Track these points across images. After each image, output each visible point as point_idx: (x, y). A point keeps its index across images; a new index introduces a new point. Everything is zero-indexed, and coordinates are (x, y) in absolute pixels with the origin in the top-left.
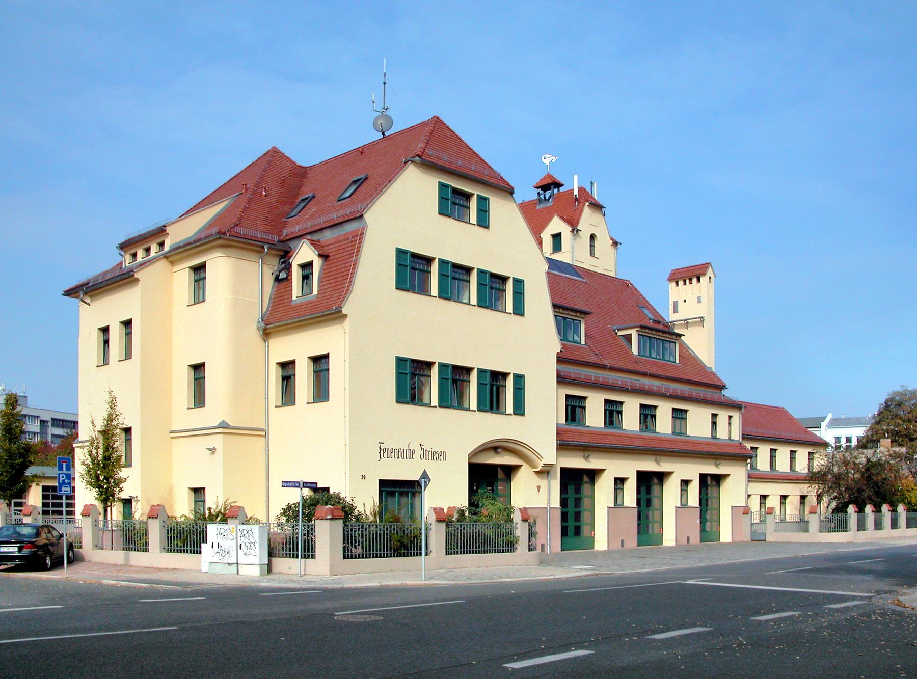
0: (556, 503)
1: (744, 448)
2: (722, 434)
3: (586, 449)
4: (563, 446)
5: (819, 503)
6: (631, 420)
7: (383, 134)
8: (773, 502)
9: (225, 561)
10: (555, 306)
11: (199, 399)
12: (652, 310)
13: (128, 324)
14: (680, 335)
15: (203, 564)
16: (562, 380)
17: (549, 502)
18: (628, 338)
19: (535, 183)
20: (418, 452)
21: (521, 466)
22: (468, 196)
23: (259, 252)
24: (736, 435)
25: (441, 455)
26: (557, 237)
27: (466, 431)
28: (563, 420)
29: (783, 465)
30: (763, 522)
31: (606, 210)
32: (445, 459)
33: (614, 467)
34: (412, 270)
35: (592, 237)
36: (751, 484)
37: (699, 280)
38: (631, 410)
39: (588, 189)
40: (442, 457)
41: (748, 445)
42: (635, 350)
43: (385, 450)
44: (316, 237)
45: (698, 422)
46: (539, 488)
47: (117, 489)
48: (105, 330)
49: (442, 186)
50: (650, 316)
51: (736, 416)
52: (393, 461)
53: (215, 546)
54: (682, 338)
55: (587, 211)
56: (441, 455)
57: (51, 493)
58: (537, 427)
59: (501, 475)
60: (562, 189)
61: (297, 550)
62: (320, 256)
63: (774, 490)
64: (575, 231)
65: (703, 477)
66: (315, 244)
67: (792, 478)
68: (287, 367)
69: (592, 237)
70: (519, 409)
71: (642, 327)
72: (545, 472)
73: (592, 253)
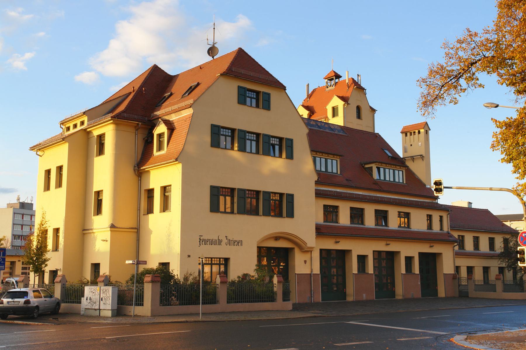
0: (317, 270)
1: (452, 236)
2: (436, 228)
6: (370, 221)
7: (213, 57)
9: (93, 308)
16: (319, 194)
20: (225, 241)
24: (446, 228)
25: (239, 243)
27: (261, 228)
29: (484, 247)
32: (241, 245)
33: (358, 248)
38: (393, 212)
39: (356, 79)
40: (240, 244)
41: (456, 234)
46: (305, 262)
47: (43, 266)
50: (390, 155)
52: (208, 246)
56: (239, 243)
60: (341, 79)
65: (421, 255)
70: (290, 214)
73: (359, 117)
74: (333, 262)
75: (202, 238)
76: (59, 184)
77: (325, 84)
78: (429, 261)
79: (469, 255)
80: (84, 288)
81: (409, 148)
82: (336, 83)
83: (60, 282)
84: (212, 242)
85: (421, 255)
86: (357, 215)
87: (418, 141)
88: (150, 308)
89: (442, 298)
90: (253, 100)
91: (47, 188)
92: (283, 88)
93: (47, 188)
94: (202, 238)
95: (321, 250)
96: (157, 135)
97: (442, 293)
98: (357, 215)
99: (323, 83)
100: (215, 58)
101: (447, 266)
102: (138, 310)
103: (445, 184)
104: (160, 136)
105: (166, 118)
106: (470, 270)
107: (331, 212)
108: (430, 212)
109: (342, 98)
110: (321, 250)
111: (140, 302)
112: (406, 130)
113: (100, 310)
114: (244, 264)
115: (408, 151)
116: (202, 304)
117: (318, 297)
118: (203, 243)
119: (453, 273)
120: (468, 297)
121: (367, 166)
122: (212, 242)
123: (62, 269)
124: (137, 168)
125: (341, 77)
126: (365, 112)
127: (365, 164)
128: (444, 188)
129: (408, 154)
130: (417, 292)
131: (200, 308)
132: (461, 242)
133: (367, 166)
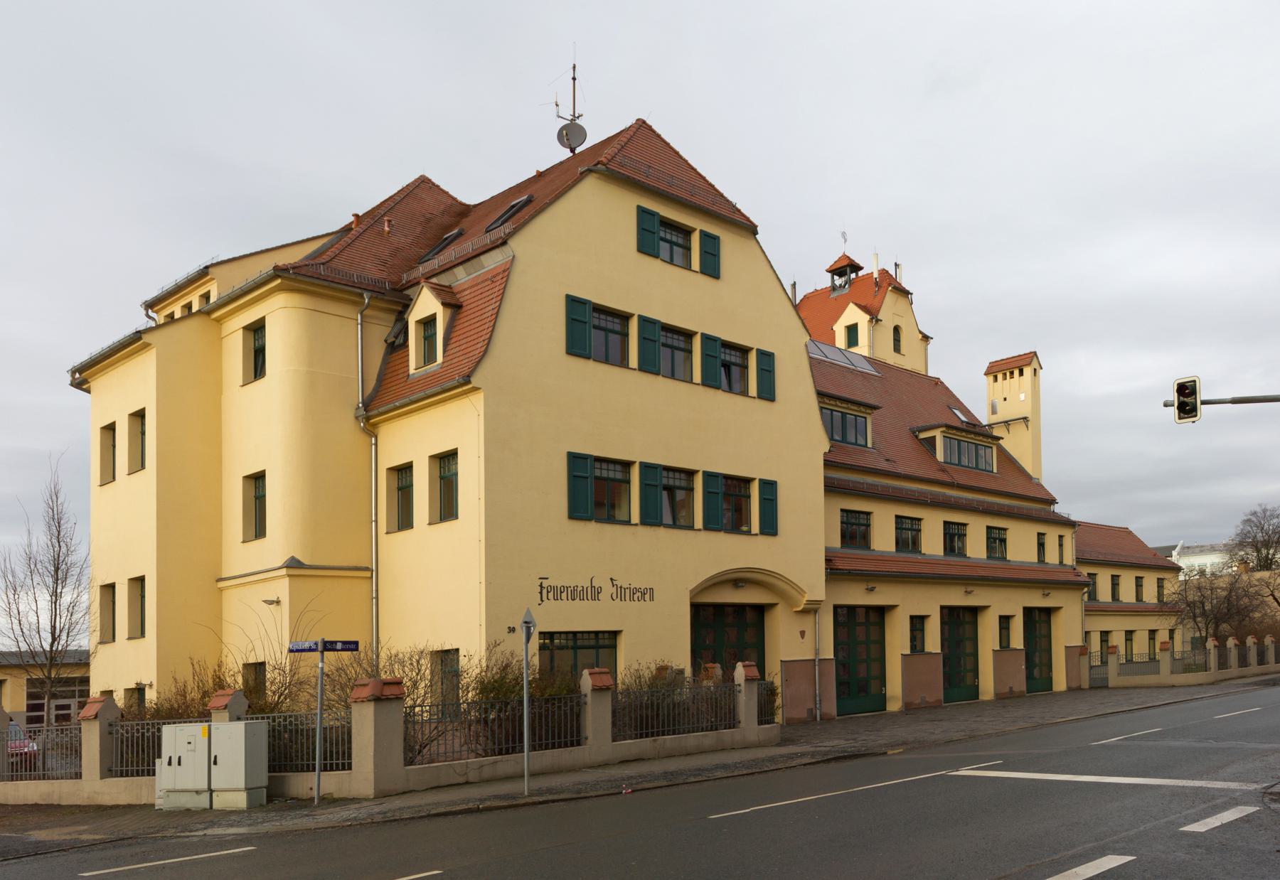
2: (1052, 557)
3: (871, 577)
4: (835, 572)
5: (1171, 638)
7: (572, 151)
8: (1118, 640)
10: (820, 394)
11: (257, 526)
12: (966, 411)
13: (140, 415)
14: (999, 438)
15: (158, 793)
16: (832, 488)
17: (817, 652)
18: (932, 441)
19: (828, 267)
20: (608, 590)
21: (776, 604)
22: (687, 232)
23: (354, 303)
24: (1069, 559)
25: (645, 594)
26: (852, 331)
27: (692, 558)
28: (836, 543)
29: (1127, 594)
30: (1104, 662)
31: (914, 298)
32: (652, 599)
33: (907, 602)
34: (593, 329)
35: (897, 330)
36: (1088, 618)
37: (1021, 373)
39: (892, 272)
40: (647, 597)
41: (1085, 571)
42: (940, 456)
43: (551, 589)
44: (443, 280)
45: (1021, 544)
46: (803, 634)
48: (110, 429)
49: (642, 211)
50: (963, 418)
51: (1068, 535)
52: (565, 605)
53: (175, 761)
54: (1001, 442)
55: (890, 298)
57: (77, 688)
58: (798, 549)
59: (750, 616)
60: (861, 273)
61: (314, 759)
62: (445, 304)
63: (1117, 626)
64: (874, 319)
65: (1028, 612)
66: (440, 291)
67: (1139, 609)
68: (403, 472)
69: (897, 330)
70: (770, 526)
71: (948, 427)
72: (811, 609)
73: (897, 348)
74: (859, 629)
75: (545, 584)
76: (138, 463)
77: (829, 284)
78: (1038, 620)
79: (1104, 611)
80: (159, 730)
81: (1001, 406)
82: (849, 282)
83: (96, 717)
84: (575, 594)
85: (1028, 612)
86: (908, 534)
87: (1016, 392)
88: (372, 776)
89: (1060, 693)
90: (677, 352)
91: (109, 475)
92: (751, 229)
93: (109, 475)
94: (545, 584)
95: (836, 607)
96: (418, 322)
97: (1060, 682)
98: (908, 534)
99: (825, 281)
100: (578, 150)
101: (1068, 628)
102: (331, 782)
103: (1203, 395)
104: (429, 323)
105: (443, 280)
106: (1105, 635)
107: (855, 531)
108: (1042, 529)
109: (865, 309)
110: (836, 607)
111: (339, 758)
112: (994, 369)
113: (211, 791)
114: (656, 641)
115: (999, 409)
116: (533, 748)
117: (831, 707)
118: (551, 595)
119: (1080, 644)
120: (1107, 687)
121: (923, 435)
122: (575, 594)
123: (155, 683)
124: (362, 412)
125: (861, 268)
126: (907, 339)
127: (920, 431)
128: (1204, 403)
129: (1000, 417)
130: (1019, 682)
131: (526, 759)
132: (1089, 585)
133: (923, 435)
